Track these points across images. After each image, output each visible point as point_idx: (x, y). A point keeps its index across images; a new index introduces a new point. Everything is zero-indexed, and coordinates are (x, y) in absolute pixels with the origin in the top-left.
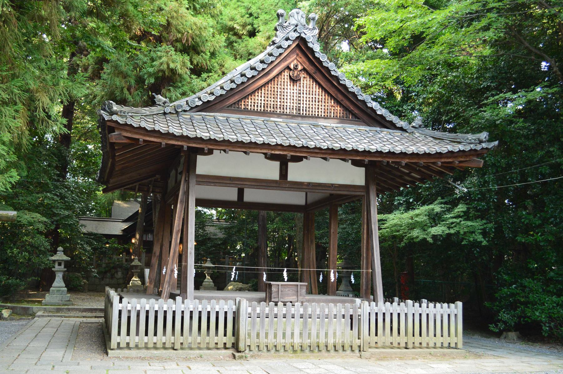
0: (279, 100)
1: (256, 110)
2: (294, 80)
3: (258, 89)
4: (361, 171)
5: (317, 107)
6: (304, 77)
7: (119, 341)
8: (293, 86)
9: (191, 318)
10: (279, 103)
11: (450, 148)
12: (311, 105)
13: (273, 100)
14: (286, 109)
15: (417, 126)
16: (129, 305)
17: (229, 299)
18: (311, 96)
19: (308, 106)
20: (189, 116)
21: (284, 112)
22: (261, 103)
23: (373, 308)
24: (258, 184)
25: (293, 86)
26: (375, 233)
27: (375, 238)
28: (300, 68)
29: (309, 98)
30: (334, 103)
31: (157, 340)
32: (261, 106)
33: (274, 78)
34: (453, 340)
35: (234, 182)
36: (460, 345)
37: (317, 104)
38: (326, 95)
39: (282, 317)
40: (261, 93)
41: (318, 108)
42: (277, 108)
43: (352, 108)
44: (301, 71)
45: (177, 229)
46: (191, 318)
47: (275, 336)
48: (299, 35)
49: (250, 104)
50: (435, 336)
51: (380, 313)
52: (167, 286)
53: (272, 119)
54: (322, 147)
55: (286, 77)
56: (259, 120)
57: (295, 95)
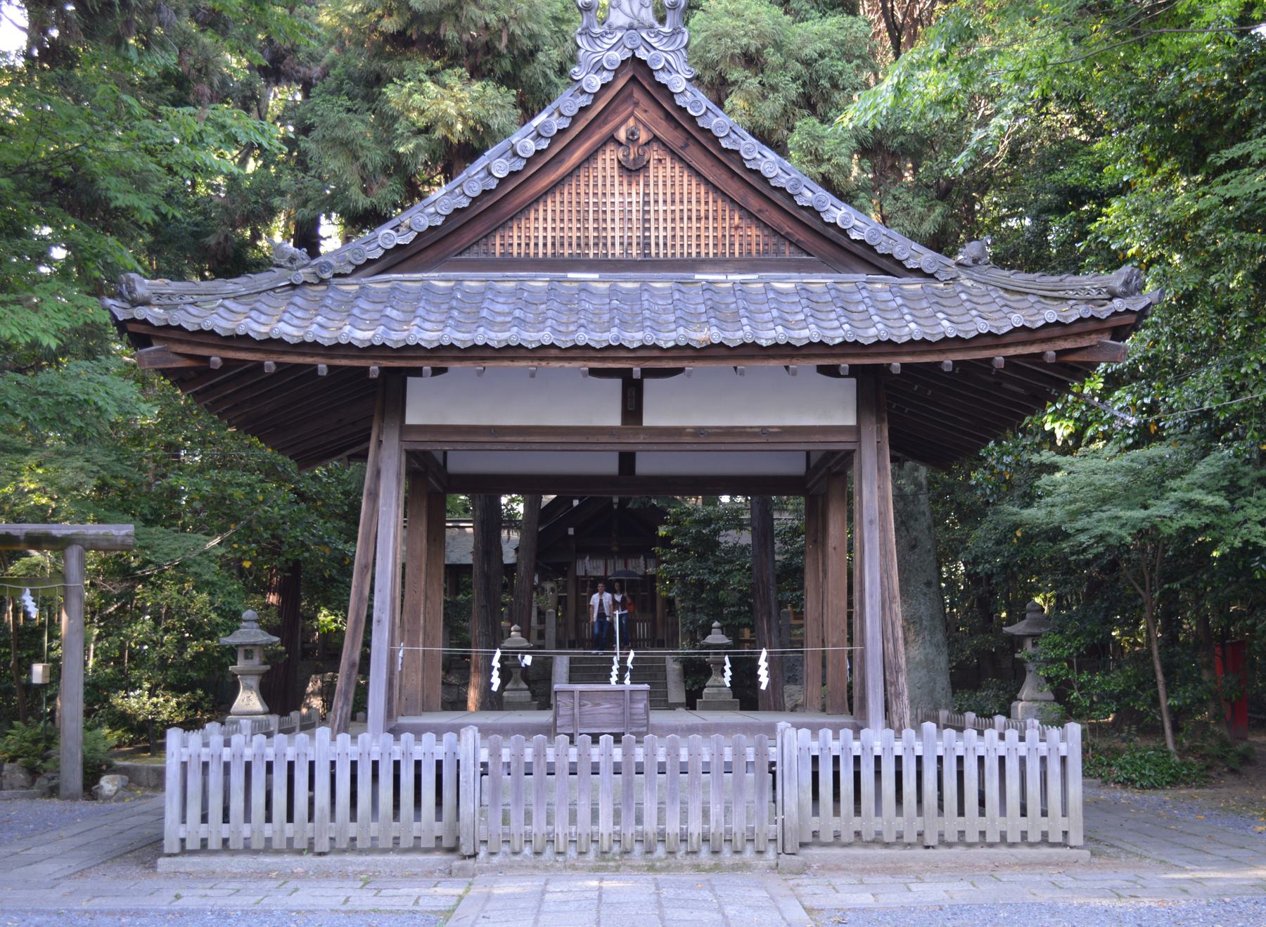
1: (532, 254)
2: (632, 170)
3: (537, 201)
4: (847, 389)
5: (694, 233)
6: (660, 161)
7: (182, 836)
8: (630, 184)
10: (592, 234)
11: (1051, 315)
12: (678, 229)
13: (575, 225)
14: (613, 244)
15: (970, 262)
16: (205, 750)
17: (426, 731)
20: (357, 287)
21: (606, 255)
22: (545, 237)
23: (825, 742)
24: (564, 440)
25: (630, 184)
26: (870, 549)
27: (870, 567)
28: (643, 136)
31: (253, 832)
32: (545, 245)
33: (578, 167)
34: (1055, 825)
35: (500, 439)
36: (1076, 838)
37: (694, 224)
38: (720, 202)
39: (567, 771)
40: (545, 211)
41: (698, 236)
42: (587, 244)
44: (647, 143)
45: (363, 562)
47: (573, 820)
49: (516, 241)
51: (846, 760)
52: (340, 704)
53: (571, 275)
54: (662, 344)
56: (540, 281)
57: (634, 208)
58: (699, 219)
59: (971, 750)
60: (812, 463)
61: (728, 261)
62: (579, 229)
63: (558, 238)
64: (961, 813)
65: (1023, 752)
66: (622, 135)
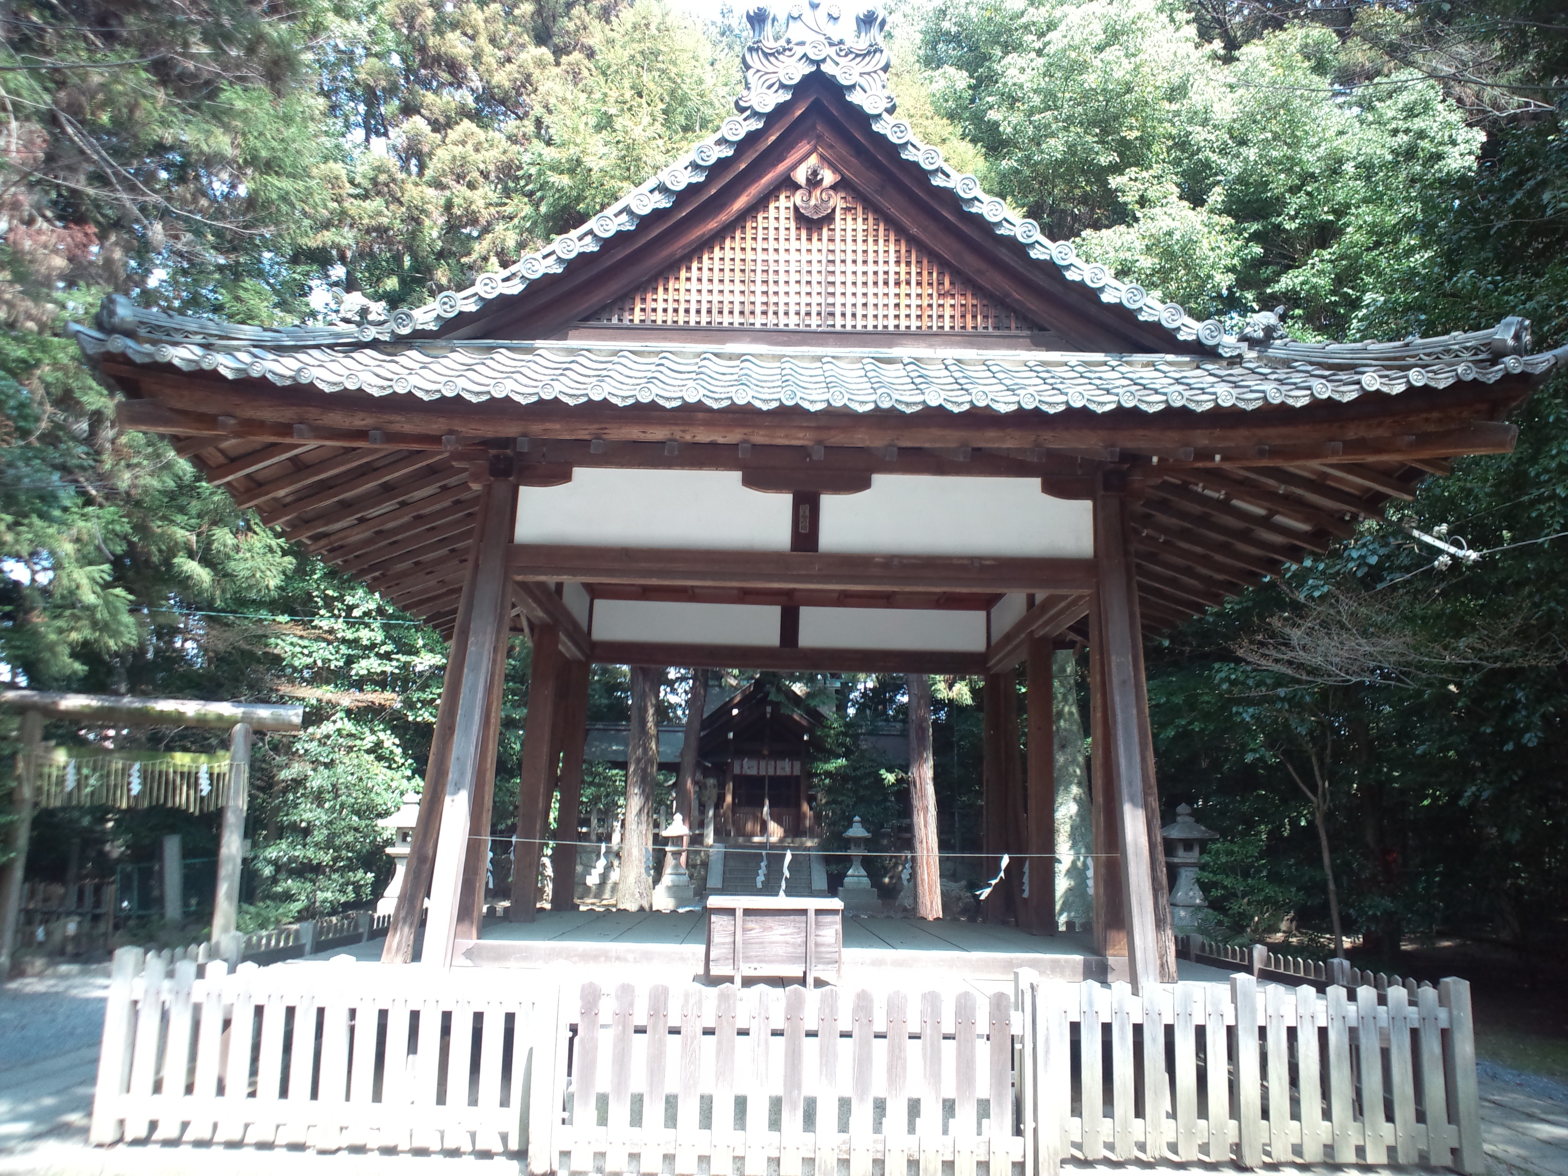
0: (759, 288)
8: (809, 239)
9: (446, 1030)
10: (759, 299)
13: (738, 287)
18: (871, 268)
19: (860, 300)
25: (809, 239)
29: (876, 273)
30: (952, 283)
43: (1017, 295)
46: (446, 1030)
48: (814, 68)
50: (158, 1087)
55: (783, 214)
58: (898, 284)
59: (1307, 1018)
60: (994, 639)
61: (935, 335)
62: (743, 292)
63: (715, 302)
64: (1295, 1115)
65: (1383, 1022)
66: (801, 175)
